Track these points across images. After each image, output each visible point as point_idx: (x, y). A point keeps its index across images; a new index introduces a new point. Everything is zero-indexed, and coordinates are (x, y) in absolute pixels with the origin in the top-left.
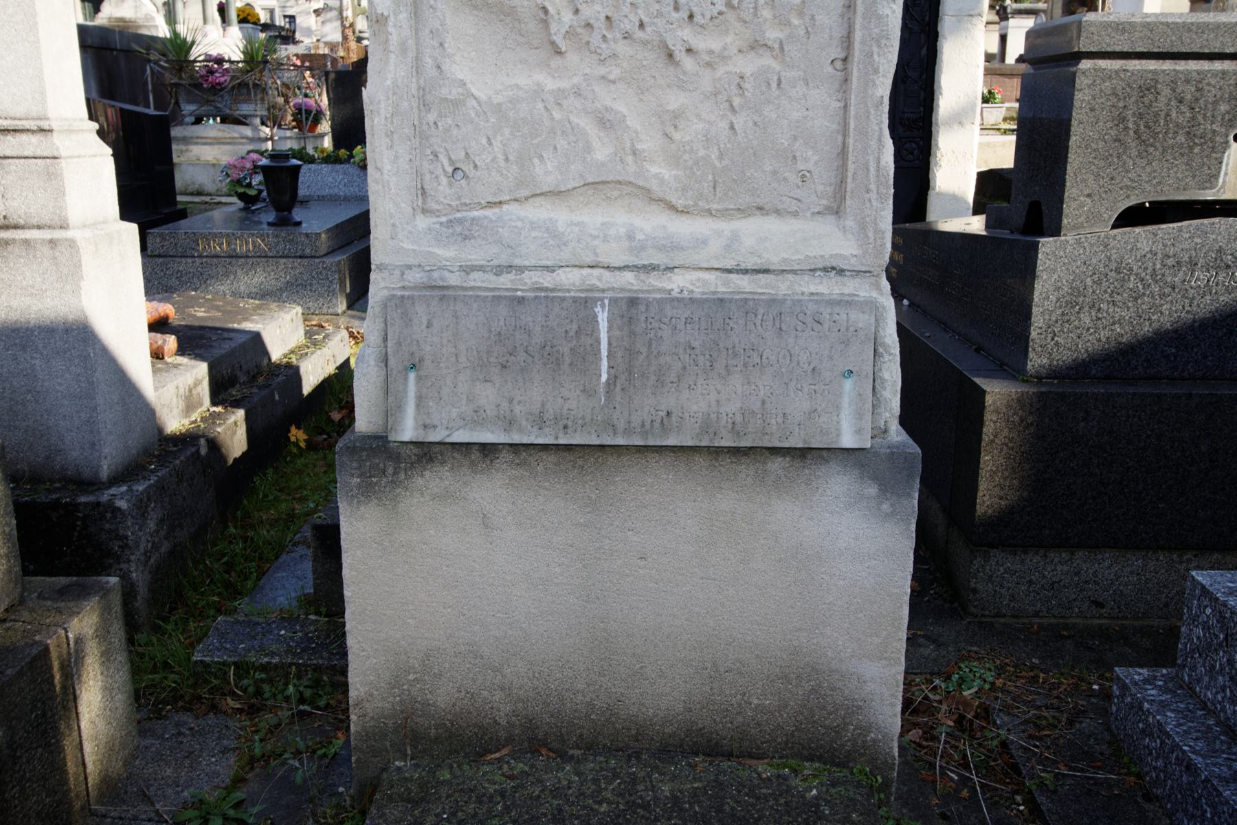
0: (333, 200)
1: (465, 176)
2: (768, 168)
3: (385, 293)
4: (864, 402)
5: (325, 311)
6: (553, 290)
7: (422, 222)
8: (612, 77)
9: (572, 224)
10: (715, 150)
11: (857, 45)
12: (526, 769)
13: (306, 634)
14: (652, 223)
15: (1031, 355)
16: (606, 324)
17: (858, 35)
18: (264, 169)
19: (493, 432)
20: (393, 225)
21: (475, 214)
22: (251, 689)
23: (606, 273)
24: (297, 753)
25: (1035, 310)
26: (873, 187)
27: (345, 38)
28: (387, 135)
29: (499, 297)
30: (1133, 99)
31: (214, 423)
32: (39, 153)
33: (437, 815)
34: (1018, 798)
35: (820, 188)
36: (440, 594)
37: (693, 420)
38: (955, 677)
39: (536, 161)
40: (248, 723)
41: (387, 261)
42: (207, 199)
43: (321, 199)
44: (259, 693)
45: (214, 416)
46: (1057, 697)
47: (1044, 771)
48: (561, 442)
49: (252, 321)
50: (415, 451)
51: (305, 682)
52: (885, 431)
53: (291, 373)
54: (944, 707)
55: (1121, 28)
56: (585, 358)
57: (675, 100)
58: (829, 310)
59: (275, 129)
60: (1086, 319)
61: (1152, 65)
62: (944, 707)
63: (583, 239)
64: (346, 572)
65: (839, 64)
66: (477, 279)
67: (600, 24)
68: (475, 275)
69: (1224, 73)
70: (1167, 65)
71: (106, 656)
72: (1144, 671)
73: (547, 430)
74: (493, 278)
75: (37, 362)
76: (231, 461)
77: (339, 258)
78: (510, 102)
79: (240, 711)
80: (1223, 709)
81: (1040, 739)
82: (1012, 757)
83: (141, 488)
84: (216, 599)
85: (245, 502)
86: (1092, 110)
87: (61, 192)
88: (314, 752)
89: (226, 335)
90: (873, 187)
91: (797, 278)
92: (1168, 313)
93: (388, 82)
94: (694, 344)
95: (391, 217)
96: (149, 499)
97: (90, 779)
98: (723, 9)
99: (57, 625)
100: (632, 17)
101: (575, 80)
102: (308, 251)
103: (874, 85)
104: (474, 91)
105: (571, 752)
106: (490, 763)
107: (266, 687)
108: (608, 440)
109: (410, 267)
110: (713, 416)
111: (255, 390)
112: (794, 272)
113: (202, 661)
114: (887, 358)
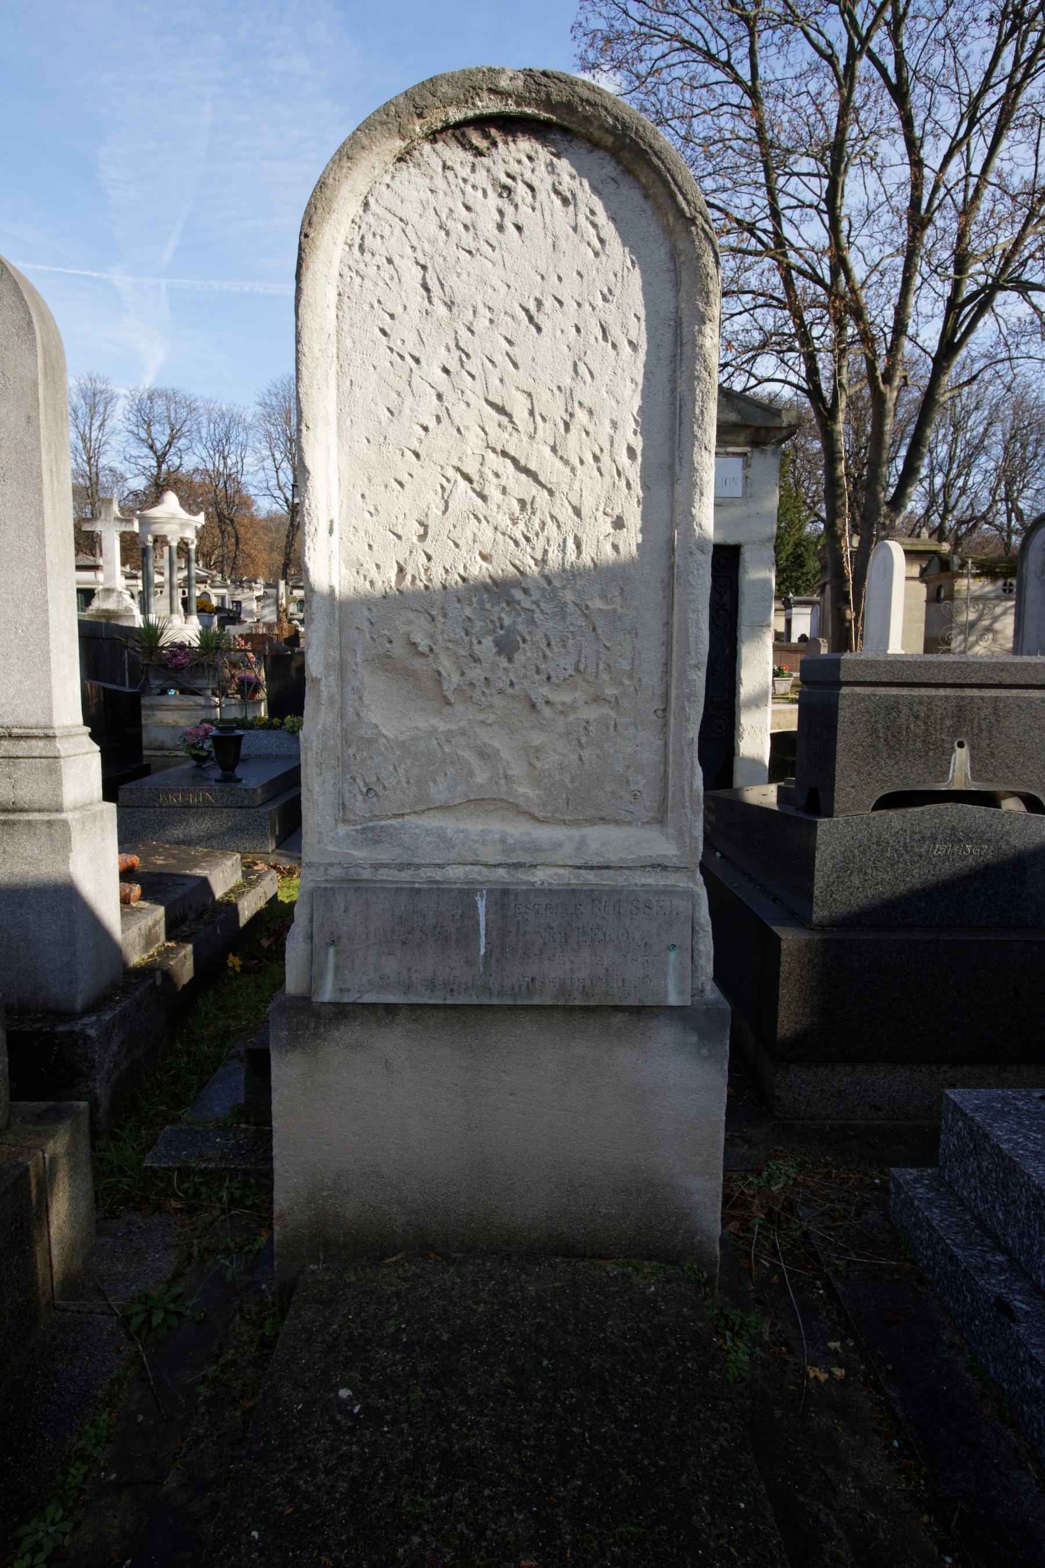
0: (267, 758)
1: (377, 795)
2: (608, 789)
3: (312, 884)
4: (684, 968)
5: (258, 850)
6: (442, 883)
7: (342, 830)
8: (489, 721)
9: (459, 831)
10: (568, 775)
11: (673, 701)
12: (418, 1271)
13: (238, 1142)
14: (518, 830)
15: (815, 909)
16: (484, 910)
17: (673, 693)
18: (214, 737)
19: (394, 995)
20: (320, 833)
21: (384, 823)
22: (191, 1191)
23: (485, 870)
24: (227, 1252)
25: (816, 874)
26: (688, 804)
27: (279, 619)
28: (317, 766)
29: (401, 889)
30: (882, 716)
31: (168, 957)
32: (44, 754)
33: (344, 1316)
34: (819, 1283)
35: (648, 804)
36: (352, 1122)
37: (552, 985)
38: (765, 1174)
39: (431, 783)
40: (187, 1222)
41: (314, 860)
42: (167, 753)
43: (258, 757)
44: (197, 1194)
45: (168, 951)
46: (847, 1191)
47: (838, 1258)
48: (449, 1002)
49: (202, 868)
50: (333, 1009)
51: (235, 1184)
52: (702, 991)
53: (230, 908)
54: (757, 1201)
55: (869, 664)
56: (467, 936)
57: (537, 739)
58: (656, 898)
59: (223, 699)
60: (856, 881)
61: (894, 691)
62: (757, 1201)
63: (468, 841)
64: (275, 1108)
65: (660, 713)
66: (384, 874)
67: (480, 683)
68: (383, 871)
69: (947, 697)
70: (905, 692)
71: (74, 1170)
72: (914, 1171)
73: (438, 993)
74: (397, 873)
75: (31, 917)
76: (180, 988)
77: (271, 808)
78: (412, 740)
79: (181, 1210)
80: (976, 1206)
81: (833, 1229)
82: (812, 1246)
83: (107, 1018)
84: (164, 1108)
85: (190, 1020)
86: (852, 723)
87: (58, 784)
88: (242, 1248)
89: (179, 881)
90: (688, 804)
91: (631, 873)
92: (918, 876)
93: (319, 727)
94: (553, 925)
95: (318, 826)
96: (113, 1027)
97: (55, 1278)
98: (573, 673)
99: (36, 1147)
100: (504, 678)
101: (461, 724)
102: (246, 803)
103: (687, 729)
104: (384, 731)
105: (454, 1255)
106: (388, 1266)
107: (203, 1189)
108: (485, 1001)
109: (332, 865)
110: (568, 981)
111: (201, 926)
112: (629, 868)
113: (151, 1167)
114: (702, 934)
